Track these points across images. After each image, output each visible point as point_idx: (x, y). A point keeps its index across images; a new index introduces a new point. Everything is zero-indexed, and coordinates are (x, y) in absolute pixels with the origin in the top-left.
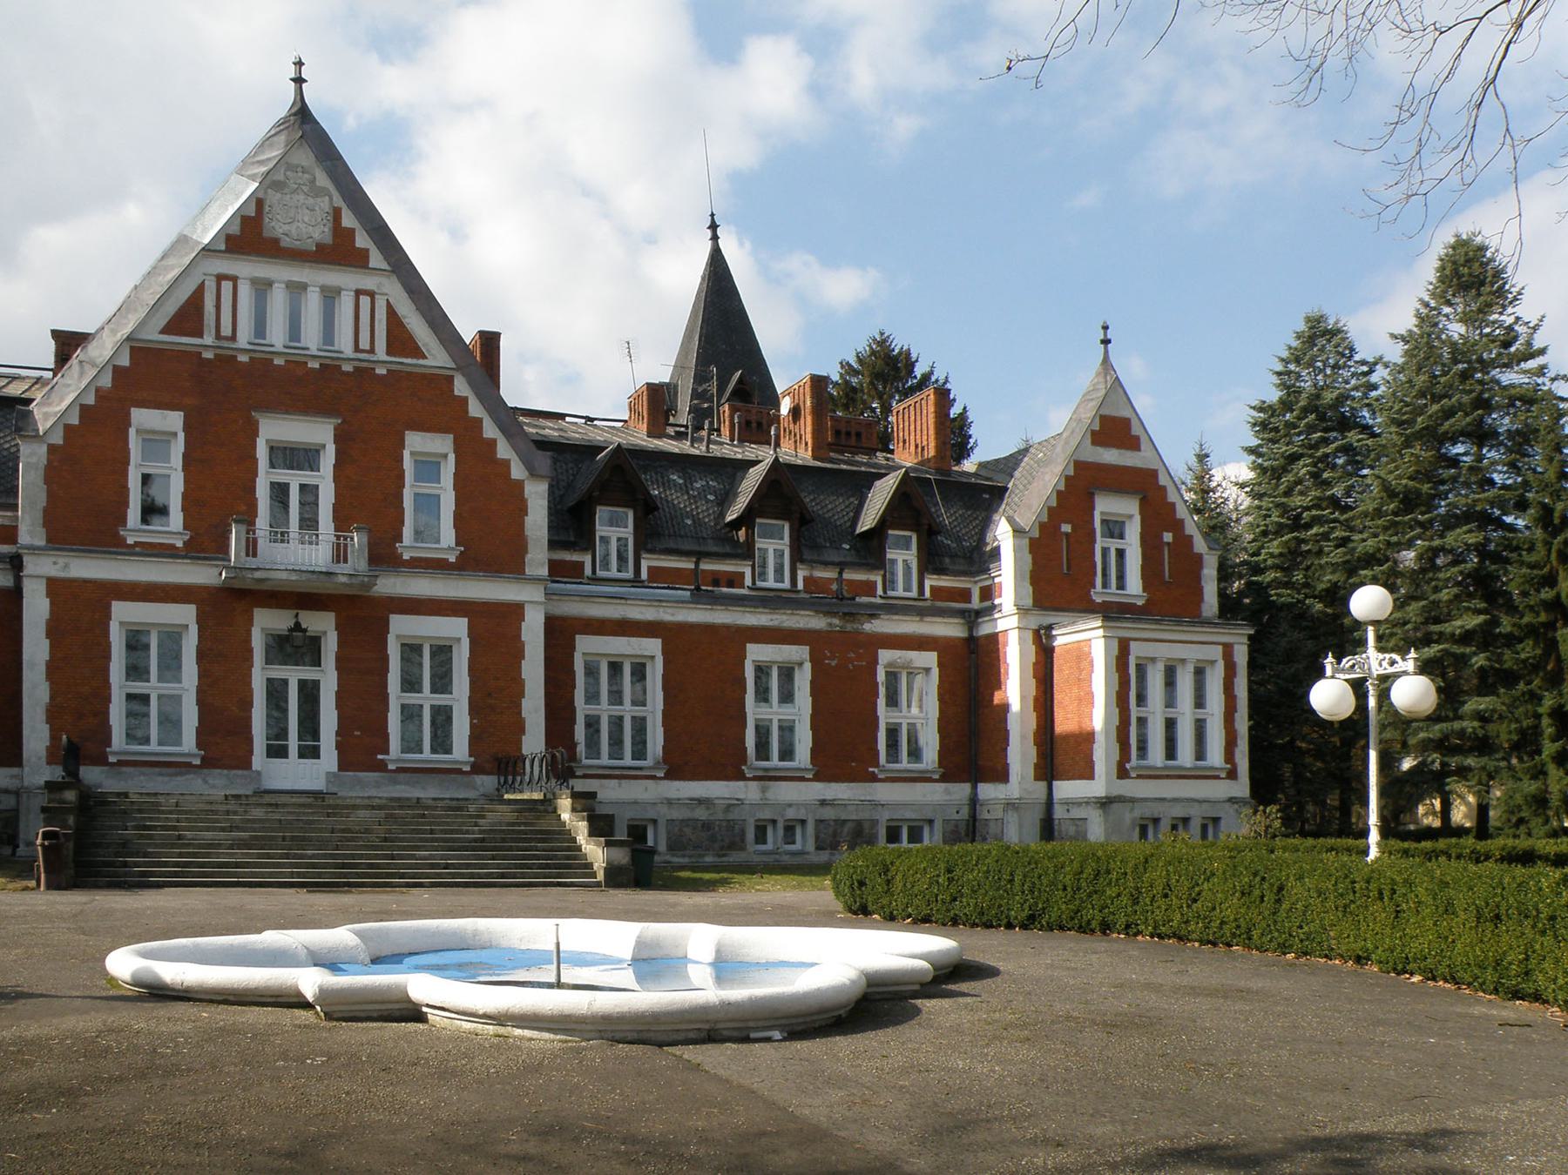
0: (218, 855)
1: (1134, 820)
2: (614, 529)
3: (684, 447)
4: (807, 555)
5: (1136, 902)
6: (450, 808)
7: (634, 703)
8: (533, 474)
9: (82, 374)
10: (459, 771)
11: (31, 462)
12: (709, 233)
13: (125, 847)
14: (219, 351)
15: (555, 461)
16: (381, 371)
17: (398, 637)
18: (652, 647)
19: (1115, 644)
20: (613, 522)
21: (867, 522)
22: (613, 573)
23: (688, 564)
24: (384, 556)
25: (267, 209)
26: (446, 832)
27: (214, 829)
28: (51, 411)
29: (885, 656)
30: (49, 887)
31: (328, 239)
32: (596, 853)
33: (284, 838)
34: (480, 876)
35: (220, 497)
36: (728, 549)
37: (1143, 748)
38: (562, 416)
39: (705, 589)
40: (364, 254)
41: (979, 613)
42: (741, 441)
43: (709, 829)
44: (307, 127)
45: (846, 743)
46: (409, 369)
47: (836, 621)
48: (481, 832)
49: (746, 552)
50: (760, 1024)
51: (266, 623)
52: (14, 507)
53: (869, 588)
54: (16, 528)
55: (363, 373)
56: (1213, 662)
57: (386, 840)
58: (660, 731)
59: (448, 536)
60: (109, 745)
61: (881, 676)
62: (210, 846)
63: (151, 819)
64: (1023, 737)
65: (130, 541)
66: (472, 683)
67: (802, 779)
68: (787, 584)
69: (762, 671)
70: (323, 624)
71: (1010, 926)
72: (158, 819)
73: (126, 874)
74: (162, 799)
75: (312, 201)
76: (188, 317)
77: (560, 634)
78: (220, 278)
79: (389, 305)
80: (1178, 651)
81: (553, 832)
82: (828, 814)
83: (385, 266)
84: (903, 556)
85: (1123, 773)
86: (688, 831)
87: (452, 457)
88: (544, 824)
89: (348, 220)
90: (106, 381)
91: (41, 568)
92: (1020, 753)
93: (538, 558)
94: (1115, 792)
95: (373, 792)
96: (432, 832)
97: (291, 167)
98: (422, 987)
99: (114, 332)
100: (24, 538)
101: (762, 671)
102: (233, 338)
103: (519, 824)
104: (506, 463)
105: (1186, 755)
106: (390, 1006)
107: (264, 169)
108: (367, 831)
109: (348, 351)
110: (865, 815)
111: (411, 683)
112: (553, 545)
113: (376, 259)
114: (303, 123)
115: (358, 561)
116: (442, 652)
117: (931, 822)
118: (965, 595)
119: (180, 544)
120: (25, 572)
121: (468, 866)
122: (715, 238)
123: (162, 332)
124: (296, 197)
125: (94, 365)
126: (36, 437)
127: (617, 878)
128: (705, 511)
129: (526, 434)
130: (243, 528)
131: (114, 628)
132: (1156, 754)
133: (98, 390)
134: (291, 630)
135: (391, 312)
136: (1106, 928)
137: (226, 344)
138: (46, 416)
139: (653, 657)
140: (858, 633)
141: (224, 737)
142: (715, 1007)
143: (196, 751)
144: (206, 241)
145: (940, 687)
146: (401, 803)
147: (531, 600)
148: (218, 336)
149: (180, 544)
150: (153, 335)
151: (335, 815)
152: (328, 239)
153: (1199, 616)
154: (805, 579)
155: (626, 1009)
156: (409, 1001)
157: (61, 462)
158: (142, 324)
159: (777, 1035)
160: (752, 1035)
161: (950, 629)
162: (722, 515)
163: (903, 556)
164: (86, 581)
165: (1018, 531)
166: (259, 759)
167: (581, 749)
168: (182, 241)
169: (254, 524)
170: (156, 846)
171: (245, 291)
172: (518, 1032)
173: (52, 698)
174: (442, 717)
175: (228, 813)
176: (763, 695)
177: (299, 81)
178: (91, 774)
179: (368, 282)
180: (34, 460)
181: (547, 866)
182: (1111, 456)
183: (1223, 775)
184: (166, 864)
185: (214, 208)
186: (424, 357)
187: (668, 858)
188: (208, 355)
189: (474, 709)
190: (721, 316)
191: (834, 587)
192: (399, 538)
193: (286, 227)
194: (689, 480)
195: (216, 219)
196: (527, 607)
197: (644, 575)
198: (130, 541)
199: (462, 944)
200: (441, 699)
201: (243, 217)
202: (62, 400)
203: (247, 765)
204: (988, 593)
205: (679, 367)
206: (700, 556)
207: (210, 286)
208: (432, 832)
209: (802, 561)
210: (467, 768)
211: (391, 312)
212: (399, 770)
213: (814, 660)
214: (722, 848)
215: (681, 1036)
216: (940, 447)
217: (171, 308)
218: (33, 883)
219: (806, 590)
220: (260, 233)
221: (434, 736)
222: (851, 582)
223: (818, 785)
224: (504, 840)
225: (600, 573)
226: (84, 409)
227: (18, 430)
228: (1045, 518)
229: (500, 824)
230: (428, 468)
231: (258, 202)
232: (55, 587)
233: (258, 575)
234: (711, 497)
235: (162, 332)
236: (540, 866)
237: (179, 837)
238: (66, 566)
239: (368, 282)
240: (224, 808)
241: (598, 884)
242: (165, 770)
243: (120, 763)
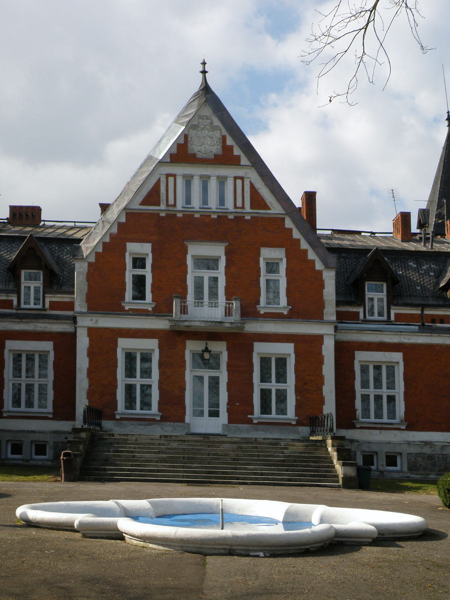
0: (150, 466)
2: (376, 295)
3: (421, 247)
6: (271, 444)
7: (388, 388)
9: (103, 227)
10: (290, 424)
11: (80, 270)
13: (107, 461)
14: (168, 212)
16: (248, 217)
17: (258, 354)
22: (376, 317)
23: (417, 312)
24: (249, 311)
25: (189, 139)
26: (266, 456)
27: (151, 453)
32: (339, 469)
33: (184, 458)
34: (278, 480)
36: (441, 302)
38: (359, 233)
40: (238, 158)
43: (432, 459)
44: (208, 96)
46: (262, 216)
48: (284, 457)
50: (256, 548)
51: (192, 347)
52: (73, 293)
55: (239, 219)
57: (234, 460)
59: (283, 300)
60: (116, 410)
62: (147, 461)
63: (122, 447)
65: (127, 308)
66: (297, 377)
70: (220, 348)
72: (125, 447)
73: (104, 475)
74: (129, 438)
75: (215, 135)
76: (153, 196)
77: (345, 352)
78: (168, 176)
81: (322, 458)
83: (248, 163)
87: (285, 260)
88: (318, 454)
89: (230, 141)
90: (115, 230)
91: (86, 322)
93: (330, 312)
96: (259, 456)
97: (201, 117)
98: (125, 525)
99: (118, 206)
100: (77, 308)
102: (175, 205)
103: (305, 453)
104: (313, 262)
106: (110, 532)
107: (187, 119)
108: (226, 455)
109: (231, 208)
112: (338, 303)
113: (244, 160)
114: (206, 94)
115: (236, 317)
116: (282, 362)
119: (150, 309)
120: (78, 325)
121: (273, 474)
123: (141, 204)
124: (204, 132)
125: (109, 222)
126: (83, 259)
127: (349, 483)
128: (428, 281)
129: (322, 244)
130: (179, 300)
131: (119, 350)
133: (111, 235)
134: (203, 351)
135: (252, 187)
137: (171, 208)
138: (87, 248)
139: (398, 363)
141: (173, 406)
143: (157, 413)
144: (160, 158)
146: (247, 441)
148: (168, 205)
149: (150, 309)
150: (136, 206)
151: (212, 446)
155: (189, 536)
156: (118, 530)
158: (131, 201)
159: (262, 554)
160: (251, 554)
162: (438, 283)
166: (188, 418)
167: (359, 412)
168: (150, 158)
169: (186, 298)
170: (121, 461)
171: (180, 182)
172: (151, 545)
173: (90, 386)
174: (282, 396)
175: (160, 444)
177: (204, 72)
178: (107, 424)
179: (240, 172)
180: (82, 270)
184: (124, 470)
186: (270, 209)
187: (408, 475)
188: (163, 214)
189: (298, 391)
192: (258, 302)
193: (199, 148)
194: (420, 265)
195: (166, 146)
196: (325, 337)
197: (393, 318)
198: (127, 308)
199: (211, 511)
200: (281, 386)
201: (178, 144)
202: (94, 240)
203: (183, 420)
205: (430, 201)
206: (423, 307)
207: (163, 179)
208: (259, 456)
210: (294, 423)
211: (252, 187)
212: (259, 423)
214: (440, 470)
215: (217, 552)
217: (144, 192)
218: (59, 479)
224: (295, 461)
225: (368, 318)
226: (105, 244)
227: (74, 256)
229: (295, 453)
230: (272, 267)
231: (185, 136)
232: (92, 332)
233: (186, 324)
234: (432, 274)
235: (141, 204)
236: (311, 476)
237: (133, 457)
238: (97, 321)
239: (240, 172)
240: (157, 442)
241: (339, 487)
242: (143, 423)
243: (122, 419)
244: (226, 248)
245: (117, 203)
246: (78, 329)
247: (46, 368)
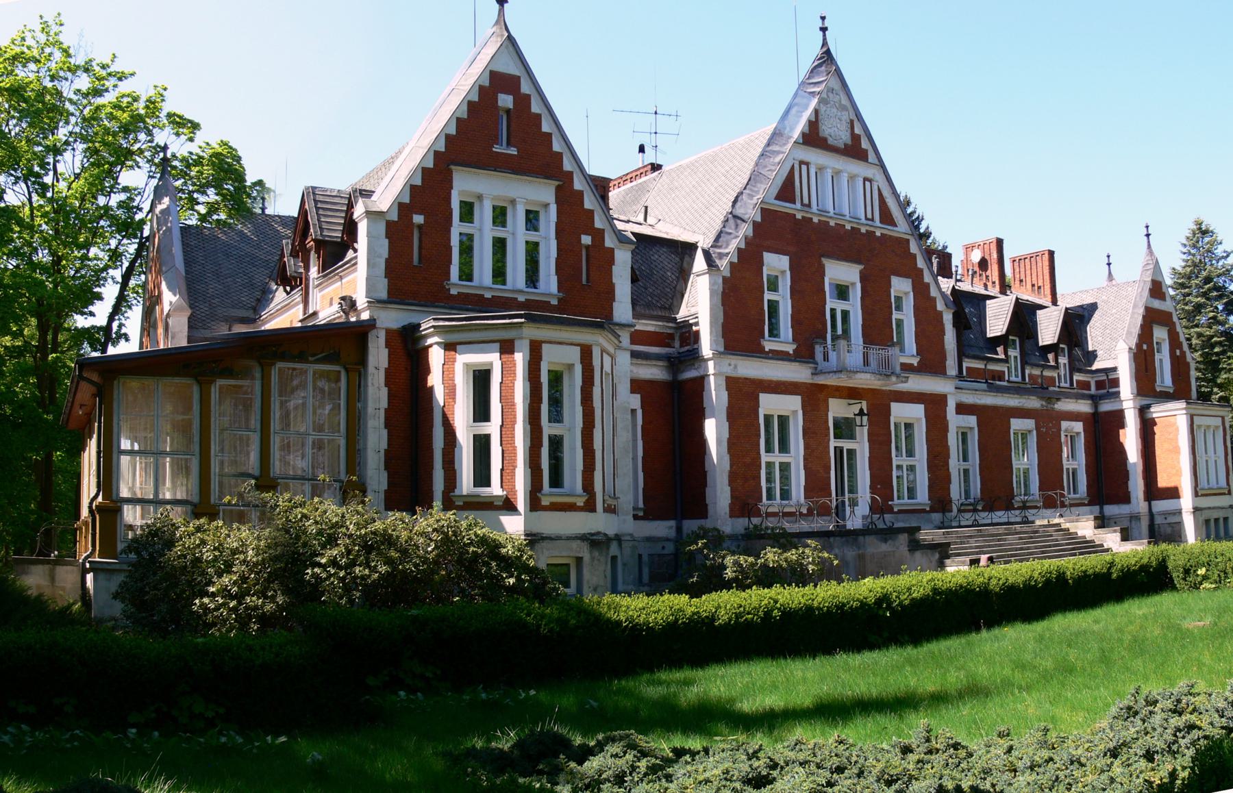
10: (924, 511)
31: (849, 142)
37: (556, 481)
76: (787, 191)
89: (858, 130)
92: (1137, 485)
148: (802, 204)
152: (849, 142)
173: (731, 466)
207: (797, 167)
220: (818, 134)
244: (861, 272)
245: (747, 191)
246: (47, 567)
247: (1117, 395)
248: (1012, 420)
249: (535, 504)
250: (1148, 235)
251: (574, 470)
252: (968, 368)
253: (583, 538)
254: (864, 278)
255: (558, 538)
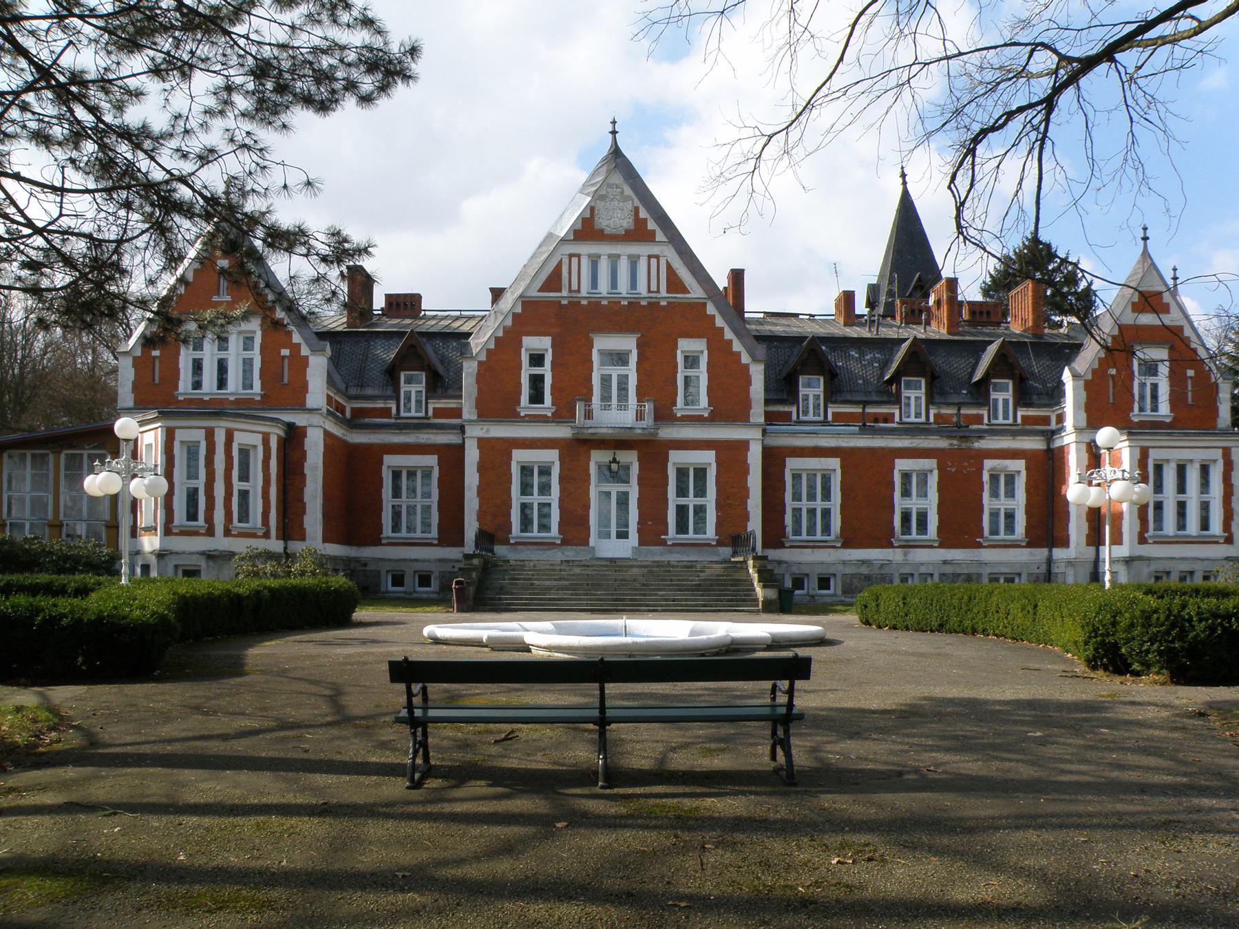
1: (1150, 574)
2: (812, 389)
4: (937, 399)
5: (986, 615)
8: (755, 359)
9: (496, 318)
10: (709, 545)
12: (901, 180)
13: (502, 590)
15: (769, 348)
16: (663, 303)
18: (834, 463)
19: (1138, 451)
20: (809, 385)
21: (978, 376)
22: (811, 417)
23: (858, 410)
24: (664, 415)
28: (479, 343)
29: (989, 464)
30: (458, 611)
35: (574, 388)
36: (885, 398)
37: (244, 517)
39: (868, 425)
40: (653, 233)
41: (1053, 433)
42: (907, 323)
45: (961, 523)
47: (955, 442)
49: (896, 400)
51: (598, 457)
52: (460, 397)
53: (979, 419)
54: (461, 409)
55: (653, 305)
56: (1215, 461)
58: (839, 517)
59: (704, 401)
61: (986, 477)
64: (1078, 517)
66: (717, 491)
67: (931, 547)
68: (923, 419)
69: (906, 476)
70: (630, 458)
71: (907, 629)
76: (553, 281)
77: (774, 459)
78: (571, 256)
79: (668, 263)
80: (1184, 455)
82: (948, 570)
83: (665, 239)
84: (1003, 395)
85: (1142, 540)
86: (856, 581)
87: (706, 352)
89: (643, 214)
90: (509, 322)
91: (475, 432)
93: (757, 413)
94: (1137, 554)
95: (657, 559)
97: (610, 186)
99: (513, 293)
100: (466, 416)
101: (906, 476)
102: (579, 291)
104: (739, 354)
105: (1193, 527)
107: (594, 189)
109: (644, 293)
110: (973, 570)
111: (682, 492)
112: (767, 402)
113: (660, 236)
115: (648, 421)
116: (701, 473)
117: (1020, 575)
118: (1046, 420)
122: (904, 183)
123: (539, 291)
130: (582, 404)
132: (1170, 526)
135: (669, 267)
136: (974, 631)
140: (970, 449)
141: (575, 526)
142: (365, 605)
145: (1027, 484)
146: (659, 564)
147: (752, 436)
148: (570, 291)
150: (534, 293)
153: (1215, 428)
154: (935, 415)
157: (486, 371)
161: (1034, 444)
162: (882, 375)
163: (1003, 395)
164: (498, 439)
165: (1075, 376)
166: (592, 541)
167: (789, 529)
168: (550, 236)
176: (906, 493)
177: (614, 133)
178: (500, 550)
179: (655, 250)
181: (732, 600)
182: (1148, 319)
183: (1222, 541)
185: (567, 214)
188: (565, 302)
189: (719, 506)
190: (908, 234)
191: (955, 419)
192: (675, 404)
194: (862, 354)
197: (830, 418)
203: (586, 543)
204: (1061, 418)
205: (881, 276)
206: (865, 404)
209: (933, 403)
211: (669, 267)
212: (674, 545)
213: (941, 468)
216: (1035, 321)
219: (935, 423)
221: (695, 523)
222: (966, 415)
223: (942, 551)
225: (802, 418)
226: (497, 339)
228: (1096, 366)
230: (692, 361)
232: (483, 443)
233: (591, 431)
235: (539, 291)
238: (488, 431)
239: (655, 250)
241: (759, 611)
243: (517, 544)
248: (671, 452)
249: (227, 532)
250: (1145, 239)
251: (256, 513)
252: (834, 414)
253: (203, 553)
254: (641, 346)
255: (183, 553)
